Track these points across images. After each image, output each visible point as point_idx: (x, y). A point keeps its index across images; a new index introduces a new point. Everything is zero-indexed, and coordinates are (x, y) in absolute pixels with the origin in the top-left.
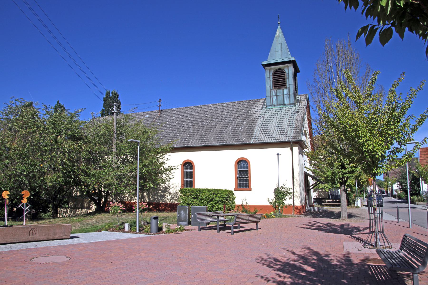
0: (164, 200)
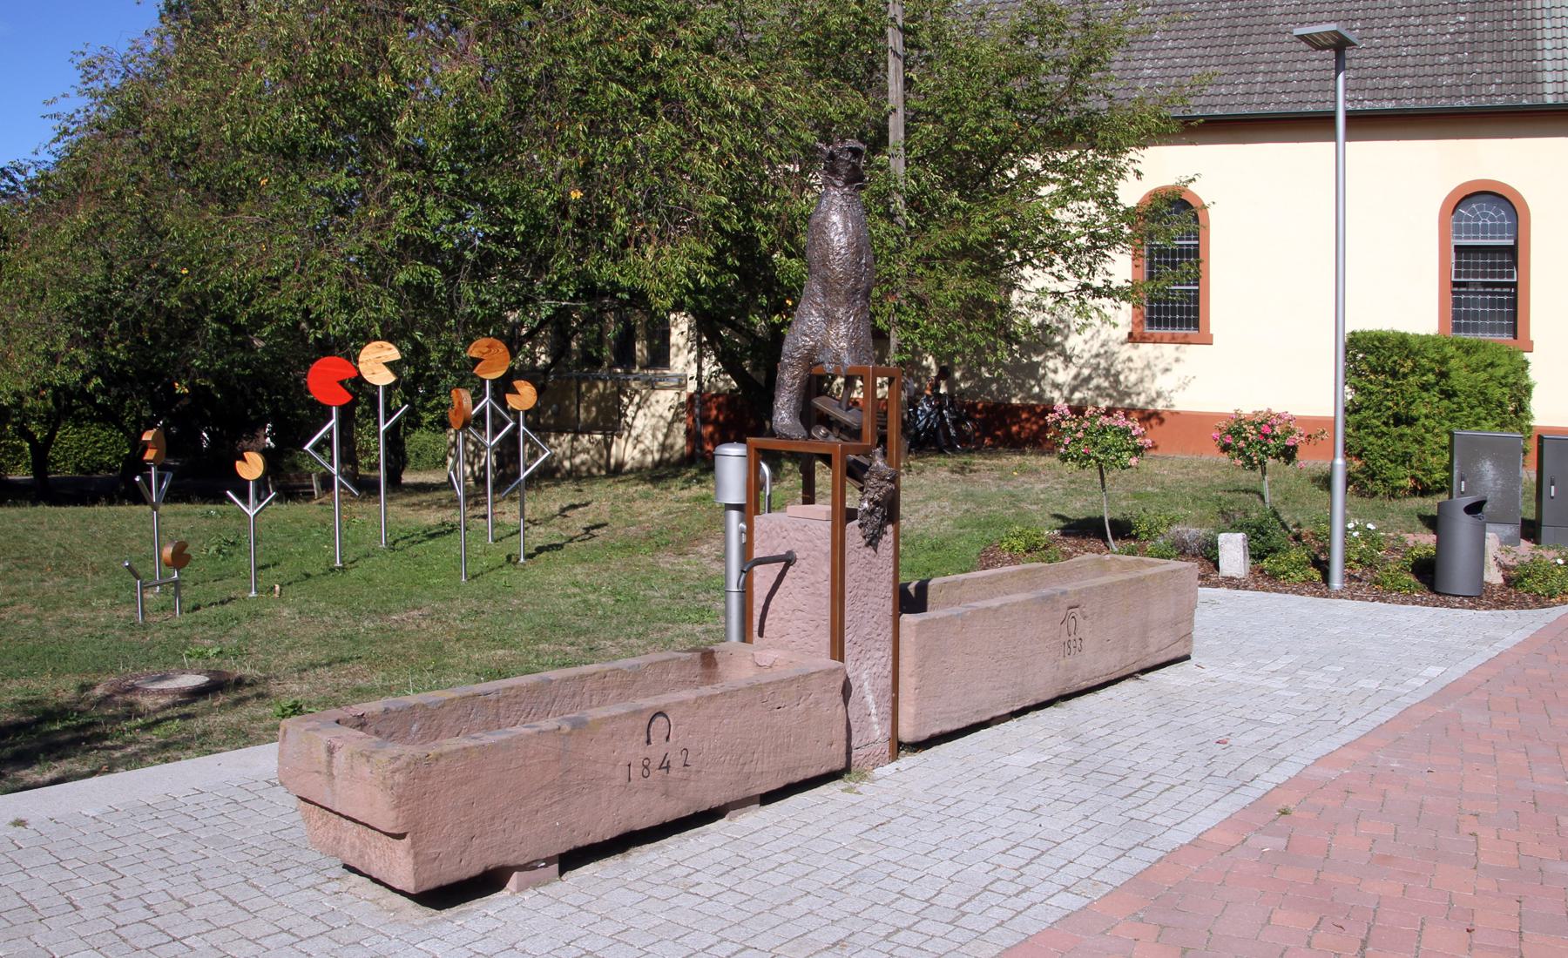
0: (1036, 390)
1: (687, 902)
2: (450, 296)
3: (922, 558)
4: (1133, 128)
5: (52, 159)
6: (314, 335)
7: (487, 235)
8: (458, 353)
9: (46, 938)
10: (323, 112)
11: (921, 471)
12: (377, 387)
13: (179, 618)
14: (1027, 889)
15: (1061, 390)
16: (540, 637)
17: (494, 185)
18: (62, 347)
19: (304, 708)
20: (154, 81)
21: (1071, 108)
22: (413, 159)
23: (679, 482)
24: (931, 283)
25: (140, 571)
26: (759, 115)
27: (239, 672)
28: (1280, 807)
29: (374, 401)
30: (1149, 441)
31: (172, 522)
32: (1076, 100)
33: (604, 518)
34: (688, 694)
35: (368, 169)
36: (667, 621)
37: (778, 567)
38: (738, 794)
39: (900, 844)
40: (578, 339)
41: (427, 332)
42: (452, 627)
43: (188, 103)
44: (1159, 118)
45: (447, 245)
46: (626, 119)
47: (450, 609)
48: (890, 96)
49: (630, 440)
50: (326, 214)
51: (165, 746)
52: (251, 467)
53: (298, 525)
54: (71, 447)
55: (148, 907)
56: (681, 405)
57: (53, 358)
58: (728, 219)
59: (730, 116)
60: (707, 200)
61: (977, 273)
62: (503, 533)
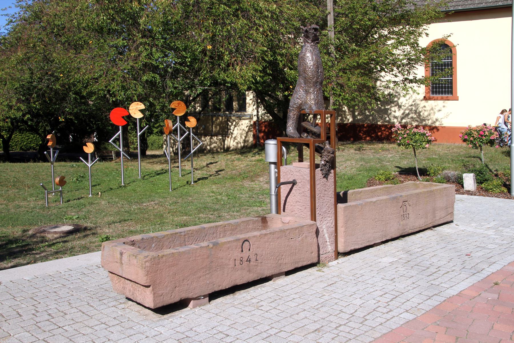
0: (387, 119)
1: (258, 313)
2: (163, 85)
3: (345, 183)
4: (425, 17)
5: (6, 32)
6: (112, 100)
7: (176, 62)
8: (167, 106)
9: (8, 327)
10: (112, 16)
11: (343, 150)
12: (136, 119)
13: (62, 205)
14: (391, 311)
15: (397, 119)
16: (200, 212)
17: (178, 44)
18: (14, 103)
19: (111, 238)
20: (45, 3)
21: (399, 10)
22: (148, 34)
23: (251, 154)
24: (346, 79)
25: (47, 187)
26: (278, 16)
27: (85, 225)
28: (494, 281)
29: (135, 124)
30: (433, 138)
31: (58, 169)
32: (401, 6)
33: (223, 167)
34: (257, 233)
35: (130, 37)
36: (248, 206)
37: (290, 186)
38: (277, 271)
39: (340, 291)
40: (211, 101)
41: (155, 99)
42: (166, 208)
43: (59, 11)
44: (436, 12)
45: (161, 66)
46: (227, 18)
47: (165, 202)
48: (328, 8)
49: (232, 138)
50: (115, 55)
51: (57, 253)
52: (89, 148)
53: (107, 170)
54: (18, 141)
55: (49, 315)
56: (251, 125)
57: (10, 107)
58: (267, 56)
59: (267, 17)
60: (259, 49)
61: (363, 74)
62: (185, 173)
